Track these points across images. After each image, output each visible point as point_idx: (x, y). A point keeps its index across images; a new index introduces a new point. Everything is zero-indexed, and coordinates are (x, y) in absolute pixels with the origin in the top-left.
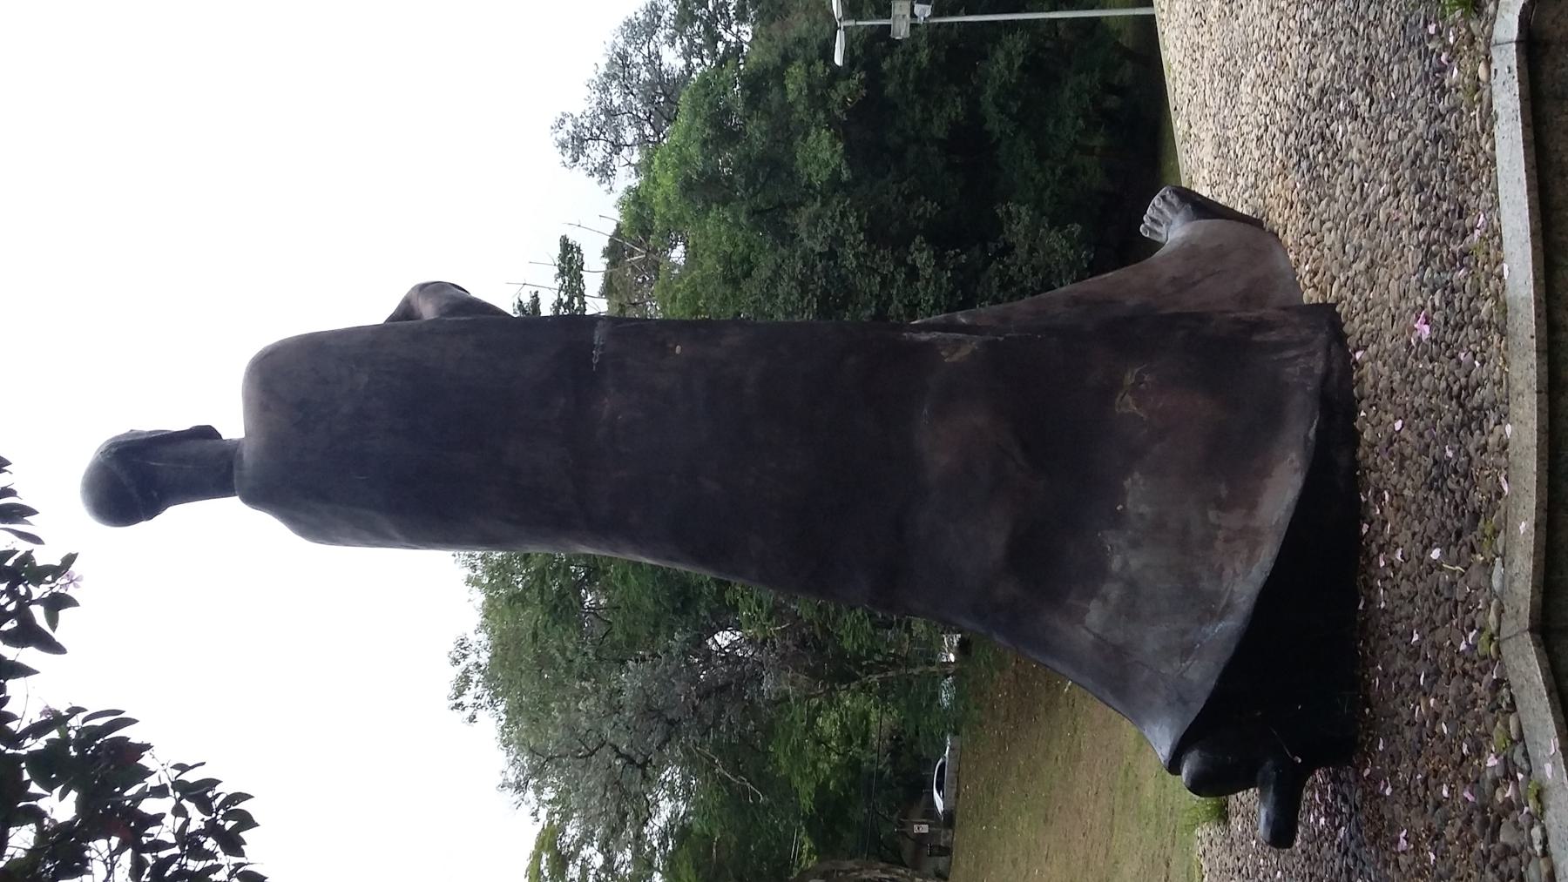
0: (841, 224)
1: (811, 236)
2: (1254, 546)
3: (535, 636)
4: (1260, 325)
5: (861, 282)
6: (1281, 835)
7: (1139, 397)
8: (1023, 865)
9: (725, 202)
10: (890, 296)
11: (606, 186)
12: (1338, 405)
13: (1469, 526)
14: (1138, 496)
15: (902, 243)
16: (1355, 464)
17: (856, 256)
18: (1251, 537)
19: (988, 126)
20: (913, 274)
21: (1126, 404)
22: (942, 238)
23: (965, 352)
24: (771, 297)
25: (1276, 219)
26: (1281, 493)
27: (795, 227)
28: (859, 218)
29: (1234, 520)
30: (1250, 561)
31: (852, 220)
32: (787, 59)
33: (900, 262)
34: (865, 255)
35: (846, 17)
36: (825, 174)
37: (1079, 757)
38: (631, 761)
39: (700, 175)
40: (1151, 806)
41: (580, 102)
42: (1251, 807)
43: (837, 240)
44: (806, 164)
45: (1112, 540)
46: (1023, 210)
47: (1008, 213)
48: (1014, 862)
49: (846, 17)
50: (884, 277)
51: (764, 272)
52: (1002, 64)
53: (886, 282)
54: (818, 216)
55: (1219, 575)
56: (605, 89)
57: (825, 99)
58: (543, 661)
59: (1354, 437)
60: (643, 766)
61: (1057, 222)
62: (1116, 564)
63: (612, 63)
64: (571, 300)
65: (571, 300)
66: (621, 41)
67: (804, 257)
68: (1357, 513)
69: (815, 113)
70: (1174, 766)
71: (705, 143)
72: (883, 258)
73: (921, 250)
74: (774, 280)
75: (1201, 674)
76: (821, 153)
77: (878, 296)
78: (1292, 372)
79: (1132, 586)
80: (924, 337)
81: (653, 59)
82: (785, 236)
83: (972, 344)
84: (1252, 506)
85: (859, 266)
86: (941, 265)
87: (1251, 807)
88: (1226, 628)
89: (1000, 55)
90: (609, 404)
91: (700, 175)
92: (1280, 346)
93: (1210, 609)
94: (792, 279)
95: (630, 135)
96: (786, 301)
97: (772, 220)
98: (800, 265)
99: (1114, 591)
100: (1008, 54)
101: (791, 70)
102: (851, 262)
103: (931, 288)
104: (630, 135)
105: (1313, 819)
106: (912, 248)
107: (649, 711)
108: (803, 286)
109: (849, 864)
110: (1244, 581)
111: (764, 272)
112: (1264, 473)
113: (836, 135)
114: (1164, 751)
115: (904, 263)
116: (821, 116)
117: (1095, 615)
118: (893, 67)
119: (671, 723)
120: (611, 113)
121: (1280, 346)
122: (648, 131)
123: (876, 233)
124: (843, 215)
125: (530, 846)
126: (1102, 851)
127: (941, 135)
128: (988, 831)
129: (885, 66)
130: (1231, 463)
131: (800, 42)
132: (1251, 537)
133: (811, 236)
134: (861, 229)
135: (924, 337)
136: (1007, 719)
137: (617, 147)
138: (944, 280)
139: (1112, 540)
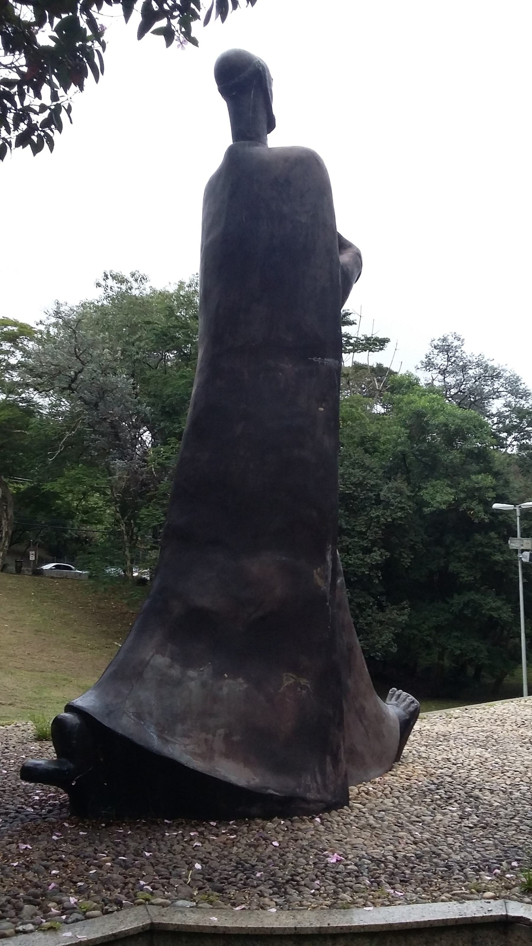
0: (397, 507)
1: (389, 490)
2: (202, 756)
3: (149, 323)
4: (336, 761)
5: (362, 519)
6: (29, 773)
7: (292, 687)
8: (10, 617)
9: (410, 437)
10: (353, 537)
11: (420, 366)
12: (288, 807)
13: (215, 887)
14: (233, 687)
15: (386, 545)
16: (252, 817)
17: (378, 517)
18: (208, 755)
19: (456, 596)
20: (367, 551)
21: (288, 680)
22: (388, 568)
23: (320, 582)
24: (353, 465)
25: (400, 770)
26: (234, 772)
27: (396, 480)
28: (401, 518)
29: (219, 745)
30: (194, 754)
31: (399, 514)
32: (496, 475)
33: (374, 543)
34: (378, 522)
35: (522, 510)
36: (427, 498)
37: (75, 651)
38: (73, 380)
39: (427, 422)
40: (46, 694)
41: (470, 350)
42: (46, 755)
43: (387, 505)
44: (433, 486)
45: (207, 671)
46: (405, 617)
47: (404, 608)
48: (12, 612)
49: (522, 510)
50: (365, 533)
51: (368, 461)
52: (494, 605)
53: (362, 535)
54: (401, 493)
55: (185, 735)
56: (478, 365)
57: (472, 498)
58: (133, 328)
59: (268, 817)
60: (70, 388)
61: (398, 638)
62: (192, 673)
63: (494, 369)
64: (351, 345)
65: (351, 345)
66: (507, 374)
67: (377, 485)
68: (223, 818)
69: (464, 492)
70: (70, 708)
71: (446, 425)
72: (376, 533)
73: (381, 555)
74: (363, 467)
75: (125, 724)
76: (440, 495)
77: (353, 530)
78: (307, 780)
79: (178, 683)
80: (329, 558)
81: (497, 394)
82: (390, 474)
83: (324, 586)
84: (227, 755)
85: (372, 518)
86: (372, 567)
87: (46, 755)
88: (153, 740)
89: (499, 603)
90: (288, 367)
91: (427, 422)
92: (323, 773)
93: (164, 731)
94: (364, 478)
95: (451, 380)
96: (350, 474)
97: (400, 466)
98: (372, 483)
99: (176, 672)
100: (499, 608)
101: (490, 477)
102: (374, 513)
103: (359, 562)
104: (451, 380)
105: (38, 792)
106: (383, 550)
107: (103, 392)
108: (359, 485)
109: (11, 512)
110: (182, 751)
111: (368, 461)
112: (247, 763)
113: (450, 504)
114: (79, 702)
115: (374, 545)
116: (462, 495)
117: (161, 661)
118: (491, 539)
119: (96, 405)
120: (464, 369)
121: (323, 773)
122: (453, 391)
123: (391, 528)
124: (402, 509)
125: (22, 320)
126: (19, 665)
127: (451, 568)
128: (31, 596)
129: (492, 534)
130: (253, 742)
131: (507, 483)
132: (208, 755)
133: (389, 490)
134: (394, 519)
135: (329, 558)
136: (99, 607)
137: (443, 372)
138: (363, 569)
139: (207, 671)
